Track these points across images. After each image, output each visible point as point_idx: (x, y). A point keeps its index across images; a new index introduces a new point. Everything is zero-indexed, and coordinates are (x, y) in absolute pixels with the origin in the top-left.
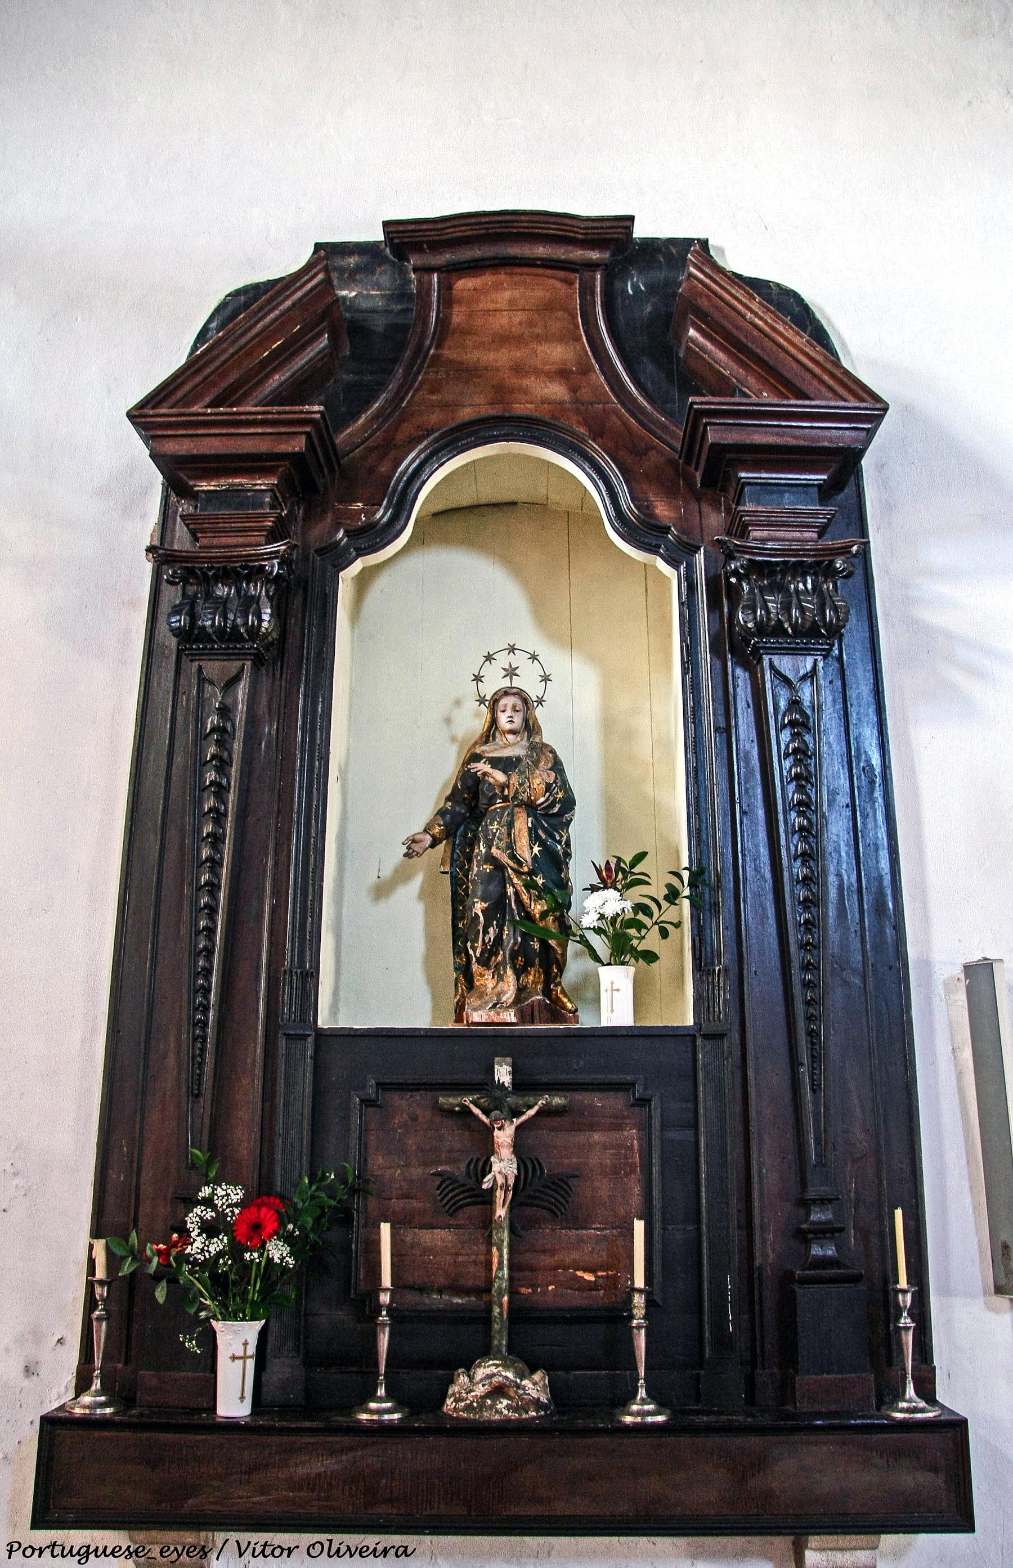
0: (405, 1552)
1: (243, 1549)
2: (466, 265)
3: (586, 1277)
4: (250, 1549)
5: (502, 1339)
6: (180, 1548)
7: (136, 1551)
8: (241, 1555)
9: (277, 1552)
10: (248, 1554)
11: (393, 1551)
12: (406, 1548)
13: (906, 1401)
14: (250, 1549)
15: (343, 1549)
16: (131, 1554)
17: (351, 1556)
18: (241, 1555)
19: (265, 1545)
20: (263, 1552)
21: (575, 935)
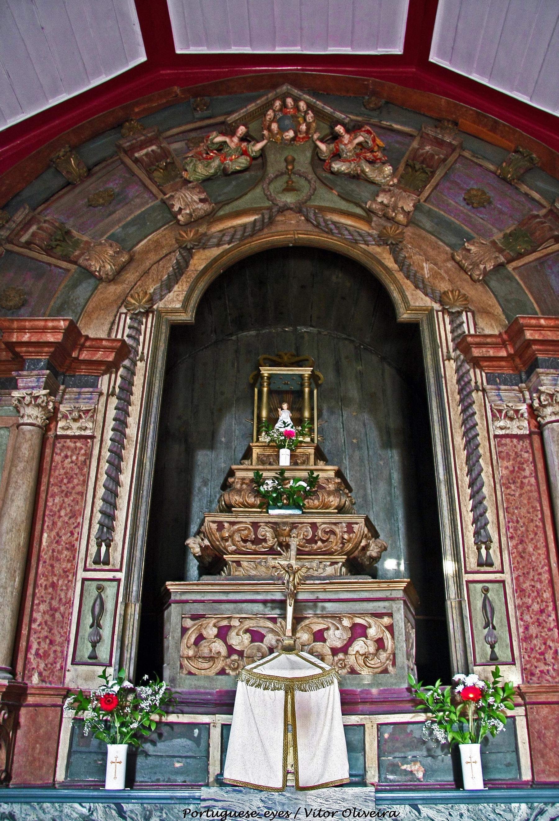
0: (394, 814)
1: (308, 812)
2: (53, 199)
3: (349, 49)
4: (312, 813)
5: (458, 575)
6: (275, 813)
7: (252, 814)
8: (307, 816)
9: (326, 814)
10: (311, 815)
11: (388, 814)
12: (395, 812)
13: (48, 344)
14: (312, 813)
15: (361, 813)
16: (249, 815)
17: (366, 816)
18: (307, 816)
19: (320, 810)
20: (319, 814)
21: (372, 800)
